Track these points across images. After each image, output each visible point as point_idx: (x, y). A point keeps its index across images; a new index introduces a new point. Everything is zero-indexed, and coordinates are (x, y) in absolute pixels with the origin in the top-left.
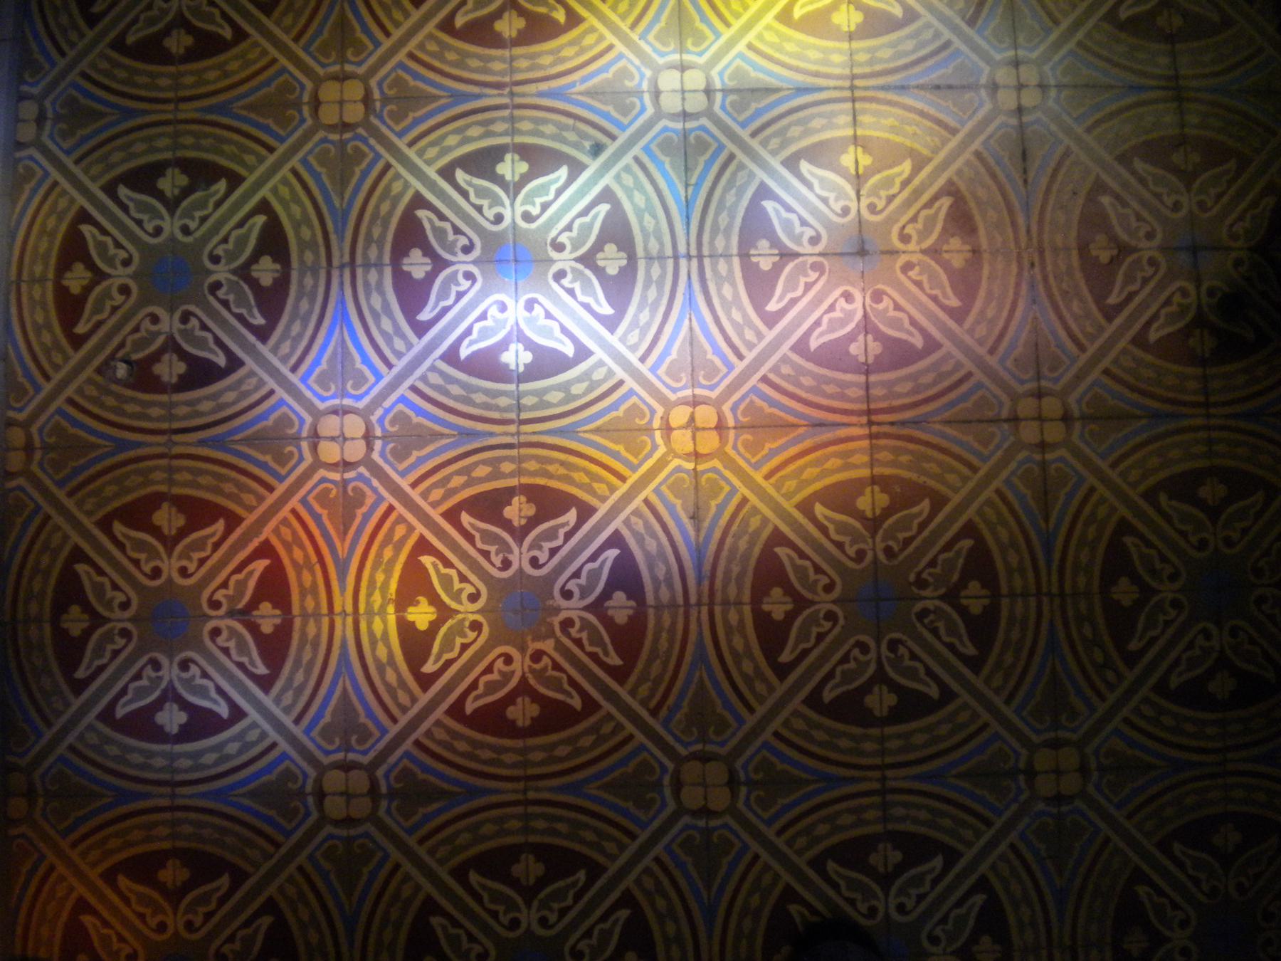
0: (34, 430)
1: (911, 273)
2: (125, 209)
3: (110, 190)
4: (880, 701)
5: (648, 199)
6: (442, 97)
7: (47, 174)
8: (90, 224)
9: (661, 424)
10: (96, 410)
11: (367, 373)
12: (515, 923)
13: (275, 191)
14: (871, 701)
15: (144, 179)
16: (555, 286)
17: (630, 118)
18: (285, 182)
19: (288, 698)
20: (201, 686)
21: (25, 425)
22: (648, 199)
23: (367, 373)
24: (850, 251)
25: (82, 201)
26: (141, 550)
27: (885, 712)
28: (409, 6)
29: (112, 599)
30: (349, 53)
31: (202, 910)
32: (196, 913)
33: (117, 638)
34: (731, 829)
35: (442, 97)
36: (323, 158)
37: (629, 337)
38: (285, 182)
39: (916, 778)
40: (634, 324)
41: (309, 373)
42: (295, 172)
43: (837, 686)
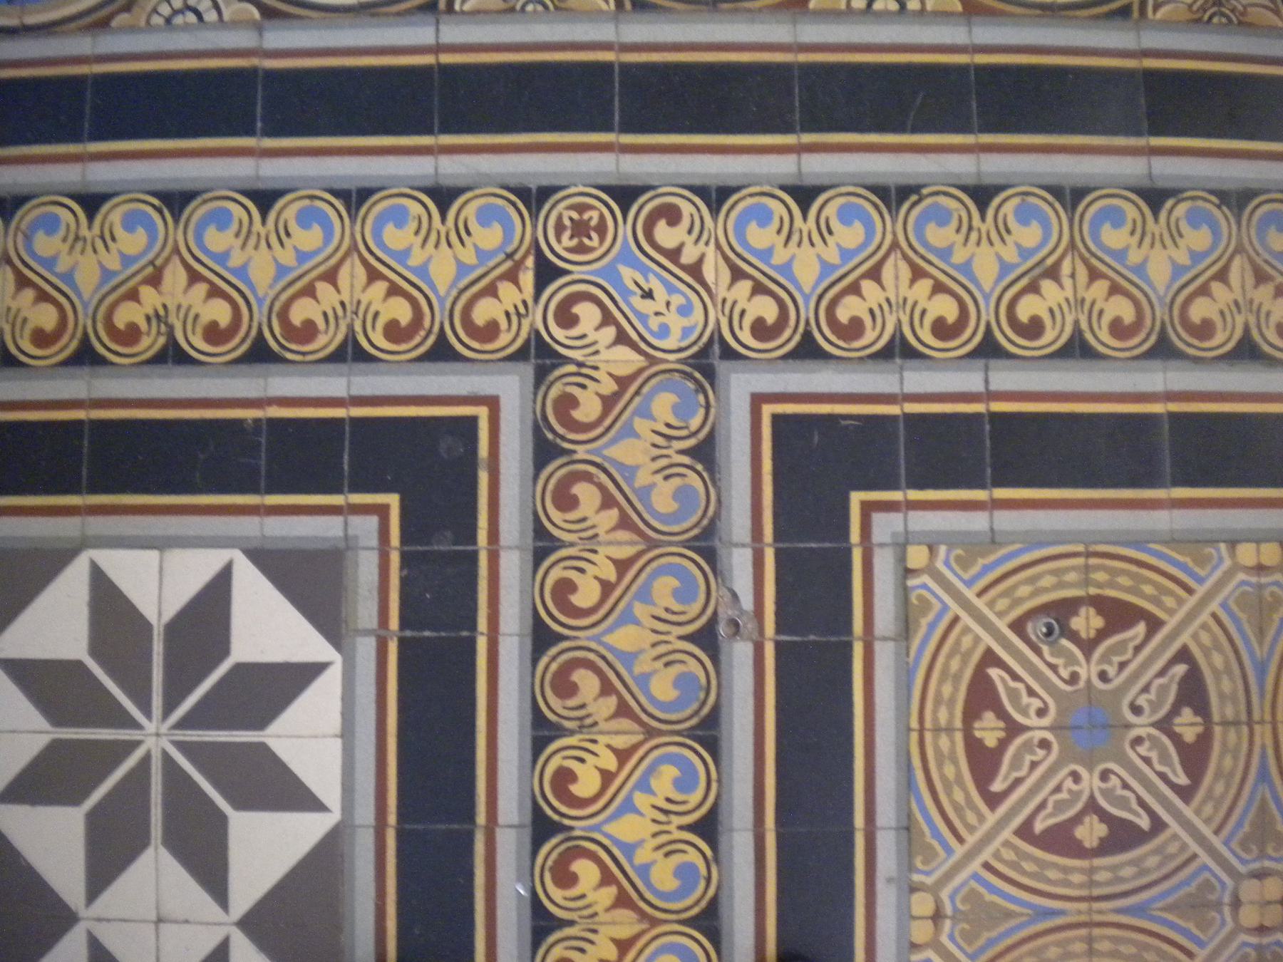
4: (989, 730)
11: (1200, 879)
12: (1105, 776)
14: (1081, 832)
16: (1065, 771)
17: (934, 600)
19: (967, 642)
20: (1123, 797)
23: (1200, 879)
27: (978, 734)
28: (628, 5)
29: (1028, 706)
30: (1212, 897)
31: (1025, 699)
32: (1028, 706)
33: (1109, 785)
34: (929, 589)
36: (1207, 886)
39: (1119, 911)
41: (939, 617)
43: (1132, 639)
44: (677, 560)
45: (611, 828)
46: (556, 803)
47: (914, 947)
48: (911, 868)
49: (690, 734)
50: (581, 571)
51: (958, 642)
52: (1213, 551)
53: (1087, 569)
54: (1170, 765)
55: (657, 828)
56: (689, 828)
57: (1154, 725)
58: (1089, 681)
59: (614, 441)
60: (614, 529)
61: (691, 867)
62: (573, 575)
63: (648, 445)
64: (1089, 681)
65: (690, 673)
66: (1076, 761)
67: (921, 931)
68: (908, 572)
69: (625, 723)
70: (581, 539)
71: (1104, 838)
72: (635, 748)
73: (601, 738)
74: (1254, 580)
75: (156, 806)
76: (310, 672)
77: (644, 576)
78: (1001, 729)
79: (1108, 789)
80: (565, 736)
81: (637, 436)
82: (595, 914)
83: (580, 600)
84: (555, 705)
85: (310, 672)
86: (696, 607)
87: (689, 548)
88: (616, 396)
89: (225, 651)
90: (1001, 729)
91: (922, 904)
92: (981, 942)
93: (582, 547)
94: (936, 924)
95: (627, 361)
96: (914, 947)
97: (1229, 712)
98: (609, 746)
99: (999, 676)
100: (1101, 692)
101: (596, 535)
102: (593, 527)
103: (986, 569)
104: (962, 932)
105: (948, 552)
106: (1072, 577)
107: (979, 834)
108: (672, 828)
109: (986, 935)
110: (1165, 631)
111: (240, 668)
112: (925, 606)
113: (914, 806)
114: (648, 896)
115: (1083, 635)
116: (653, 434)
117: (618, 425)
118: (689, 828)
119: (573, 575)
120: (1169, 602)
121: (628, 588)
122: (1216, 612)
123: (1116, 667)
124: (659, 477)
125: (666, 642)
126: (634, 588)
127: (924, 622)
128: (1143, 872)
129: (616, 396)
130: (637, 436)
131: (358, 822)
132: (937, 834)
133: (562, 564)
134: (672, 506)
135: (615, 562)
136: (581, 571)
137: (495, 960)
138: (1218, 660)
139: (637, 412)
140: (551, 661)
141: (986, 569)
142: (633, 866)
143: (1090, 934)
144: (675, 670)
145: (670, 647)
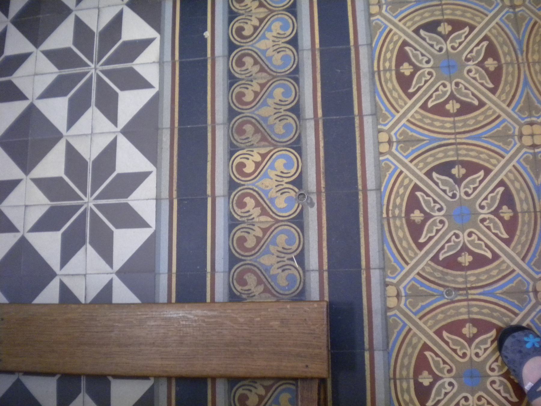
0: (378, 17)
1: (485, 223)
2: (478, 45)
3: (486, 38)
4: (406, 69)
5: (521, 185)
6: (499, 294)
7: (490, 11)
8: (469, 31)
9: (402, 298)
10: (388, 40)
13: (490, 108)
15: (491, 52)
16: (452, 233)
18: (494, 112)
21: (380, 13)
22: (521, 185)
24: (84, 280)
25: (479, 27)
26: (457, 345)
35: (499, 294)
37: (428, 268)
38: (494, 112)
40: (435, 270)
42: (499, 116)
44: (286, 227)
45: (257, 45)
46: (237, 104)
47: (381, 154)
48: (378, 123)
49: (288, 76)
50: (249, 233)
51: (411, 340)
52: (526, 296)
53: (469, 306)
54: (485, 79)
55: (277, 183)
56: (288, 42)
57: (491, 213)
58: (447, 50)
59: (259, 107)
60: (257, 7)
61: (287, 56)
62: (246, 235)
63: (276, 257)
64: (447, 50)
65: (293, 274)
66: (467, 392)
67: (384, 148)
68: (371, 15)
69: (264, 74)
70: (246, 77)
71: (471, 262)
72: (267, 83)
73: (254, 149)
74: (532, 151)
75: (94, 90)
76: (145, 175)
77: (270, 89)
78: (411, 69)
79: (484, 392)
80: (239, 16)
81: (268, 106)
82: (251, 10)
83: (246, 33)
84: (238, 212)
85: (145, 175)
86: (293, 171)
87: (289, 77)
88: (263, 209)
89: (114, 169)
90: (411, 69)
91: (384, 137)
92: (418, 307)
93: (246, 15)
94: (390, 145)
95: (266, 222)
96: (381, 154)
97: (508, 59)
98: (259, 227)
99: (430, 355)
100: (465, 200)
101: (251, 10)
102: (251, 72)
103: (413, 152)
104: (410, 302)
105: (406, 300)
106: (451, 153)
107: (415, 261)
108: (282, 110)
109: (421, 304)
110: (492, 174)
111: (119, 175)
112: (396, 323)
113: (385, 248)
114: (272, 68)
115: (468, 336)
116: (275, 105)
117: (262, 173)
118: (288, 42)
119: (246, 235)
120: (494, 161)
121: (266, 91)
122: (515, 164)
123: (483, 350)
124: (277, 120)
125: (282, 185)
126: (266, 27)
127: (396, 331)
128: (464, 12)
129: (263, 209)
130: (268, 106)
131: (165, 60)
132: (387, 110)
133: (242, 230)
134: (283, 131)
135: (262, 229)
136: (249, 233)
137: (216, 405)
138: (517, 185)
139: (267, 30)
140: (236, 194)
141: (413, 152)
142: (265, 57)
143: (442, 8)
144: (285, 196)
145: (280, 114)
